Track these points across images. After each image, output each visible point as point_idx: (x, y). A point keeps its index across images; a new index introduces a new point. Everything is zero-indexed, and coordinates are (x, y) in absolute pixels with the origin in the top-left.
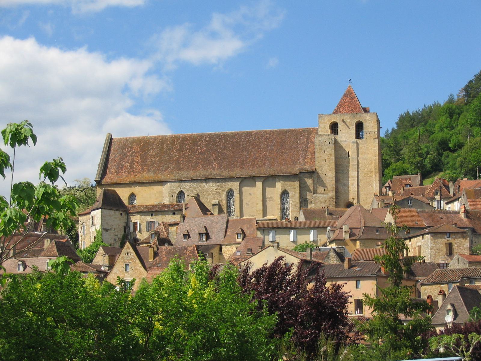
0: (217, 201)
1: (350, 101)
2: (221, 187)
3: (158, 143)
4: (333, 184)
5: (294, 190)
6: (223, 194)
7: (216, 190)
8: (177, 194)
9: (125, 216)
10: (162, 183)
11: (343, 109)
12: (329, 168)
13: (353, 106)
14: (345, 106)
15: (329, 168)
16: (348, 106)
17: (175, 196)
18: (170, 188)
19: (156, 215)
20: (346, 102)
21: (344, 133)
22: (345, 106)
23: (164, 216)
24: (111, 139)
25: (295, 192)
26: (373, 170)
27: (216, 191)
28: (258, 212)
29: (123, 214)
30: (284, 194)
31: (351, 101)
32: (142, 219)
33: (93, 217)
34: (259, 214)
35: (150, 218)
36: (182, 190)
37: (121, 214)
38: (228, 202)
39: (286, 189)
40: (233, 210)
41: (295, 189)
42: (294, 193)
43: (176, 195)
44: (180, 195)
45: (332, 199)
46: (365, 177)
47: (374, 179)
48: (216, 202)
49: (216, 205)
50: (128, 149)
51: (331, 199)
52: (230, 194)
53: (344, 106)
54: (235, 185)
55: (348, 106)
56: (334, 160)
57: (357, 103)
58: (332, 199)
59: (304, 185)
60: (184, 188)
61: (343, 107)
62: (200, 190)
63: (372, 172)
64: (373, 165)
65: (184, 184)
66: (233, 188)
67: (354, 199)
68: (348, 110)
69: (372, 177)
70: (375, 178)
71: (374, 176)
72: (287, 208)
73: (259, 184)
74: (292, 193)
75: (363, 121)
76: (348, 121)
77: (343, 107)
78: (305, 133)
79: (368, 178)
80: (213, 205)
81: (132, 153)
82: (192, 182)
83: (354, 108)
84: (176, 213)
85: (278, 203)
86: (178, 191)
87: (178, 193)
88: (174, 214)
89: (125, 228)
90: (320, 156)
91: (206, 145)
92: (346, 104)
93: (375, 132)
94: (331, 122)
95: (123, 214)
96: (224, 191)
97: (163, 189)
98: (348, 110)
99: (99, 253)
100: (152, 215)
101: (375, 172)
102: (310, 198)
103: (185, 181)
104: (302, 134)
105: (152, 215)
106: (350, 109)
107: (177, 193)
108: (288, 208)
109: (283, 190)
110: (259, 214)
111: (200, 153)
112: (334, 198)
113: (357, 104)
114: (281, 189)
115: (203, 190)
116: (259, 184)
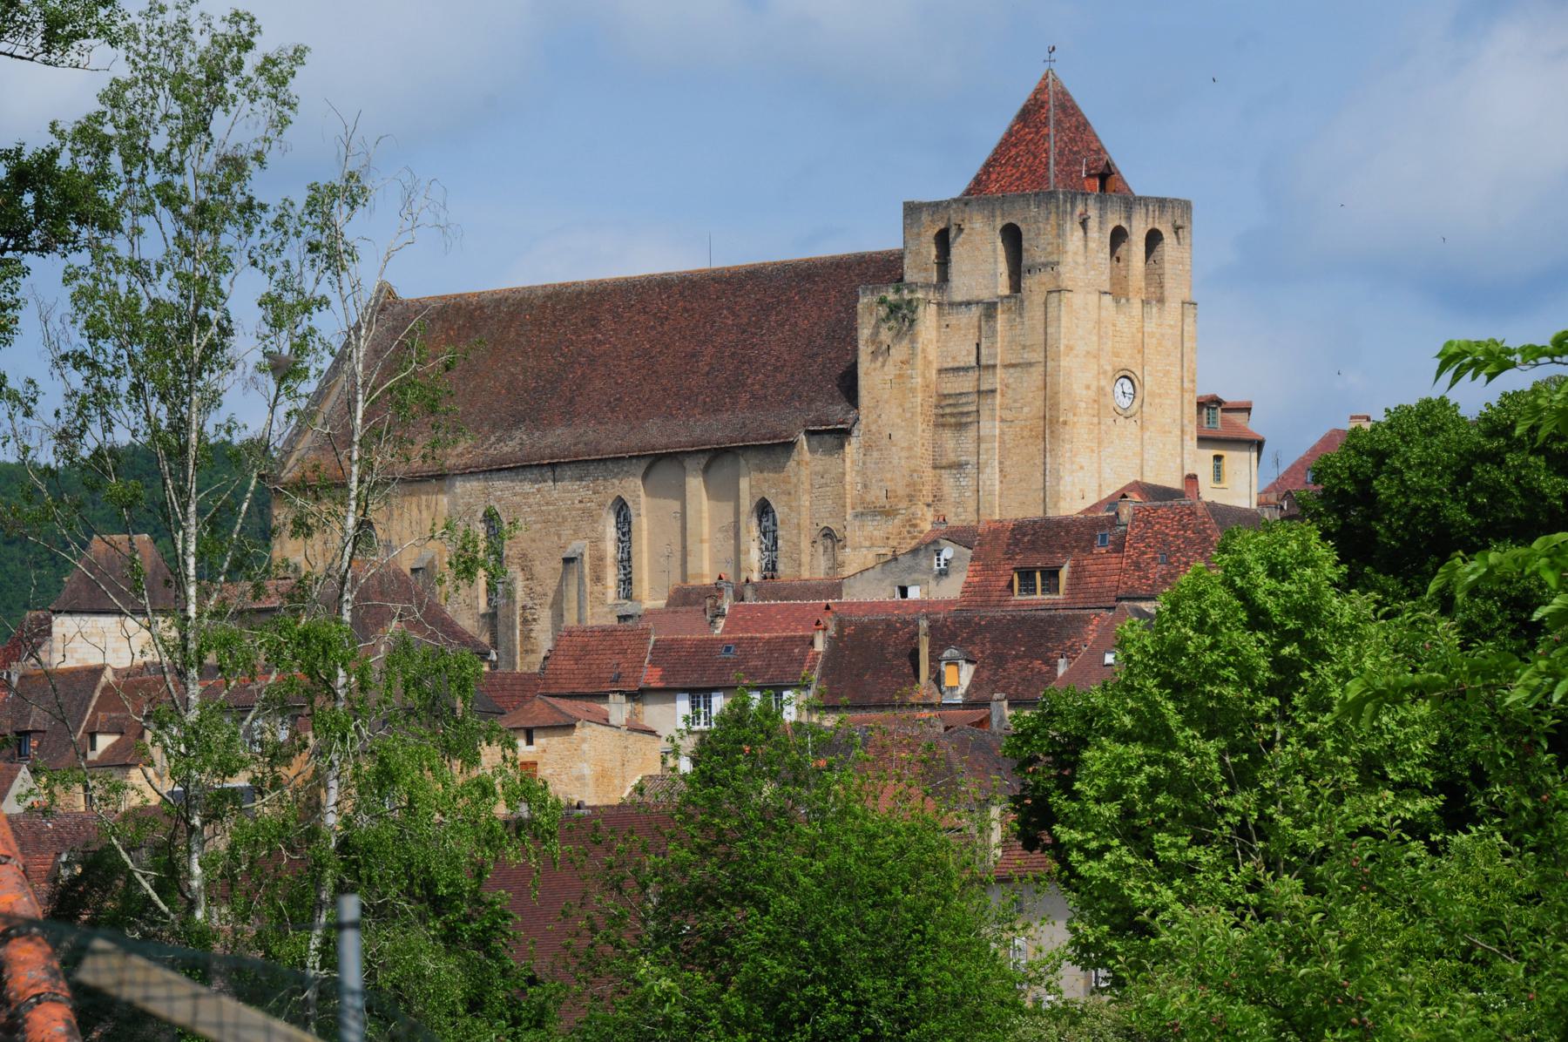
5: (785, 498)
7: (580, 502)
15: (900, 410)
27: (582, 505)
42: (786, 510)
51: (904, 526)
60: (499, 500)
83: (1030, 167)
109: (757, 499)
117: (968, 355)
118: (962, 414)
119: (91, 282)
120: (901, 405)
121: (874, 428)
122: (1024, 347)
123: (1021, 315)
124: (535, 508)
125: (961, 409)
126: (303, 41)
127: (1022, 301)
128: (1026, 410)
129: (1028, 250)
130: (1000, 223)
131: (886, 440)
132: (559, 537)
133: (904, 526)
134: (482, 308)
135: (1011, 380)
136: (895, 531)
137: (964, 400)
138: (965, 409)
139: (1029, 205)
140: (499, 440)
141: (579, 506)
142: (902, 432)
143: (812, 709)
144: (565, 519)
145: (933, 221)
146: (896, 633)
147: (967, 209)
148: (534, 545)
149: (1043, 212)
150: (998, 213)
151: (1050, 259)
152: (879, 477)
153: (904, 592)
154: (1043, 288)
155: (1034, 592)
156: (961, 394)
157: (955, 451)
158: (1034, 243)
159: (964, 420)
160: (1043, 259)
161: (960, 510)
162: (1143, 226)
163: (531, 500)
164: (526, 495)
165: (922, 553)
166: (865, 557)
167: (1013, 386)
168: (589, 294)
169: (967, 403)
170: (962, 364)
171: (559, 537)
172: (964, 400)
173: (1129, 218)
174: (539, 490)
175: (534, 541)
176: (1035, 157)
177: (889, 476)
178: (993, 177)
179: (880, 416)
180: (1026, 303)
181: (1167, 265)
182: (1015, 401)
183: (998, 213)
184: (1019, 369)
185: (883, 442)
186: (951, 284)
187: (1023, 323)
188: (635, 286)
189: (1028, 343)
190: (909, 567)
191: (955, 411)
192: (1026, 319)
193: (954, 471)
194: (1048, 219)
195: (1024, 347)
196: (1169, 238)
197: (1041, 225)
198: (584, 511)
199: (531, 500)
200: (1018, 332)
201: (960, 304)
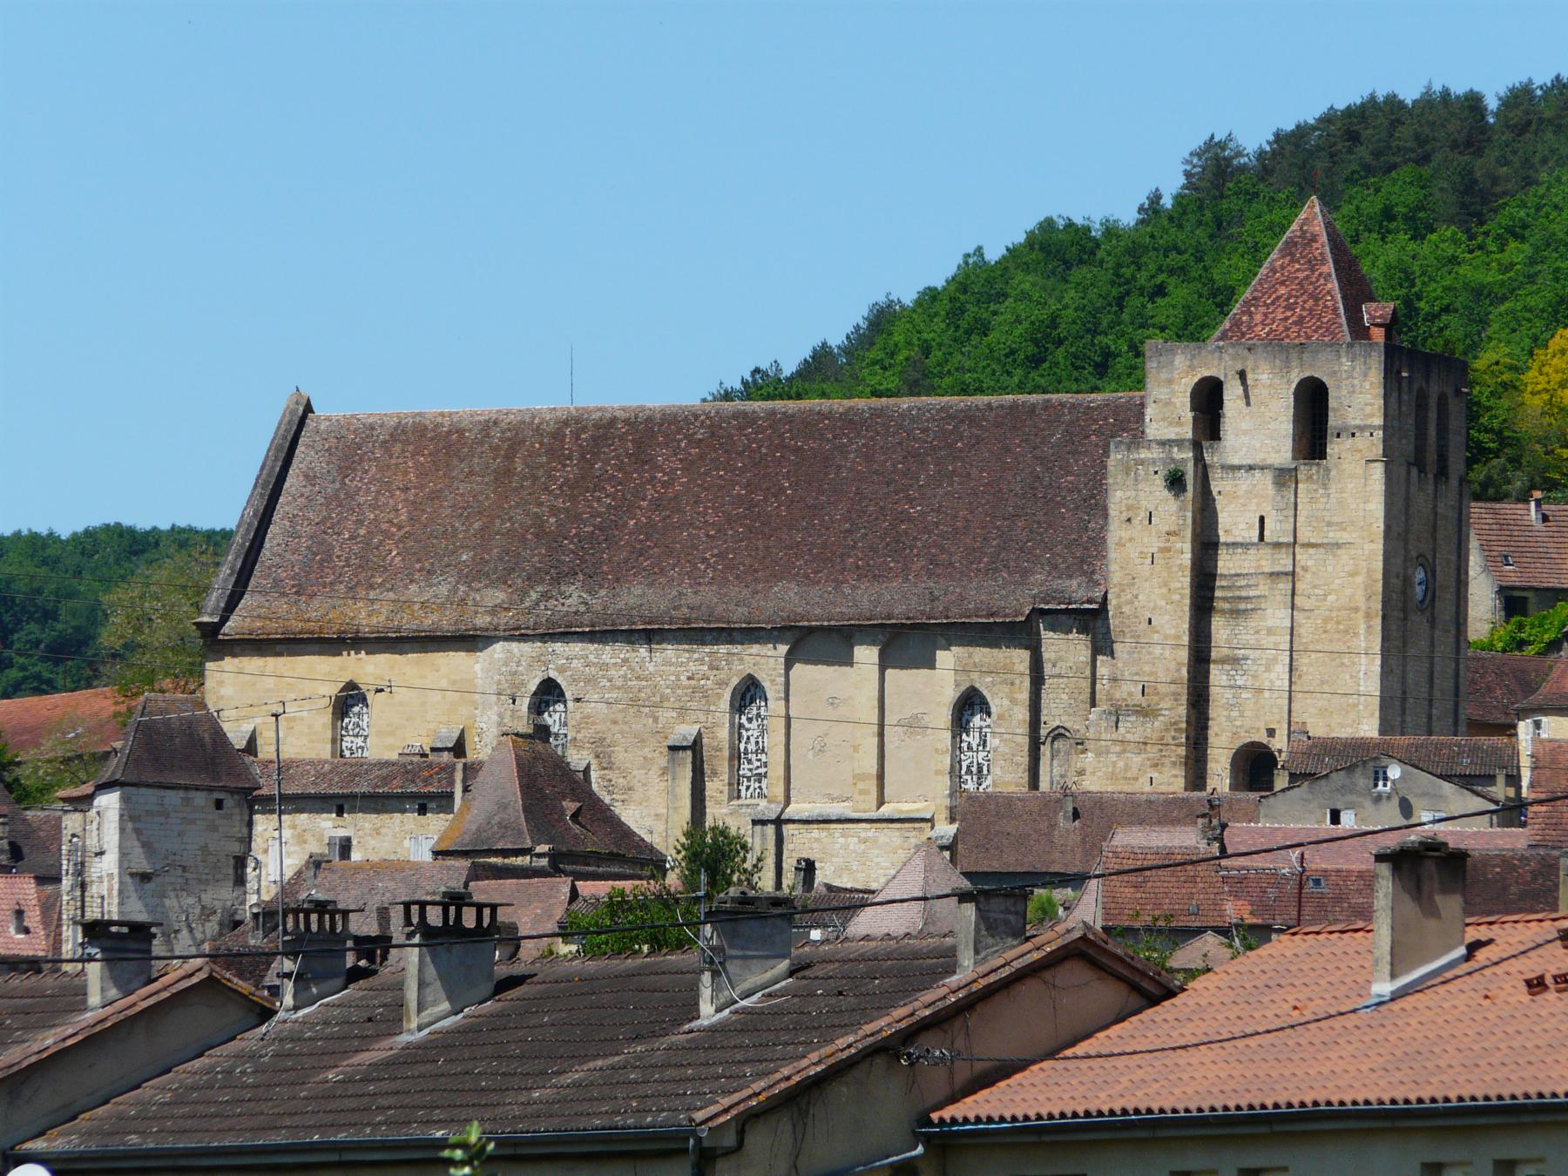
0: (694, 729)
2: (711, 668)
3: (495, 449)
5: (1006, 689)
6: (720, 696)
7: (689, 678)
8: (535, 694)
9: (237, 811)
10: (470, 641)
11: (1265, 315)
12: (1164, 590)
14: (1278, 298)
15: (1164, 590)
16: (1287, 299)
17: (524, 704)
18: (506, 664)
19: (352, 811)
20: (1283, 283)
21: (1245, 432)
23: (385, 817)
24: (308, 408)
25: (1014, 701)
26: (1361, 601)
27: (693, 682)
28: (861, 786)
29: (229, 802)
30: (969, 704)
31: (1307, 278)
32: (299, 830)
33: (98, 813)
34: (862, 792)
35: (329, 824)
36: (553, 674)
37: (219, 804)
38: (740, 735)
40: (762, 770)
41: (1012, 684)
42: (1006, 702)
43: (527, 701)
44: (546, 698)
45: (1173, 733)
46: (1325, 632)
48: (685, 731)
49: (684, 748)
50: (366, 472)
51: (1167, 730)
52: (748, 693)
53: (1273, 303)
54: (765, 661)
55: (1287, 299)
56: (1187, 558)
58: (1173, 733)
59: (1054, 666)
60: (561, 670)
61: (1268, 306)
62: (625, 677)
63: (1356, 609)
64: (1360, 579)
65: (558, 647)
66: (760, 676)
67: (1271, 733)
68: (1287, 319)
69: (1356, 634)
71: (1362, 628)
73: (866, 655)
74: (997, 701)
76: (1266, 376)
77: (1268, 306)
79: (1336, 636)
80: (673, 749)
81: (378, 492)
82: (592, 641)
83: (1311, 310)
84: (432, 805)
85: (939, 746)
86: (537, 681)
87: (538, 688)
88: (422, 810)
90: (1131, 539)
91: (688, 466)
92: (1283, 291)
93: (1375, 428)
94: (1196, 380)
95: (229, 802)
96: (722, 684)
97: (477, 667)
98: (1287, 319)
100: (340, 813)
101: (1368, 616)
103: (566, 636)
104: (1096, 421)
105: (340, 813)
106: (1295, 318)
107: (534, 689)
108: (985, 772)
109: (963, 688)
110: (862, 792)
111: (657, 505)
113: (1329, 293)
114: (957, 685)
115: (638, 678)
116: (866, 655)
118: (1240, 598)
122: (1329, 524)
123: (1325, 487)
124: (619, 683)
125: (1238, 593)
126: (1555, 74)
127: (1328, 470)
128: (1330, 598)
129: (1335, 410)
130: (1296, 377)
132: (656, 720)
133: (1167, 730)
134: (461, 432)
135: (1310, 563)
137: (1243, 582)
140: (546, 596)
141: (687, 683)
143: (1393, 976)
144: (664, 698)
145: (1192, 368)
148: (616, 728)
149: (1359, 367)
151: (1369, 422)
153: (1335, 818)
154: (1358, 456)
156: (1237, 575)
159: (1242, 606)
160: (1358, 422)
161: (1235, 714)
163: (612, 672)
164: (605, 667)
167: (1314, 569)
168: (627, 422)
169: (1248, 586)
170: (1239, 539)
171: (656, 720)
172: (1243, 582)
173: (1427, 382)
174: (625, 661)
175: (615, 722)
176: (1317, 300)
177: (1147, 668)
178: (1258, 318)
180: (1333, 473)
182: (1315, 587)
184: (1322, 550)
185: (1141, 627)
186: (1223, 443)
188: (696, 417)
189: (1335, 519)
193: (1228, 667)
194: (1366, 375)
196: (1232, 395)
197: (1356, 382)
198: (695, 690)
199: (612, 672)
201: (1239, 468)
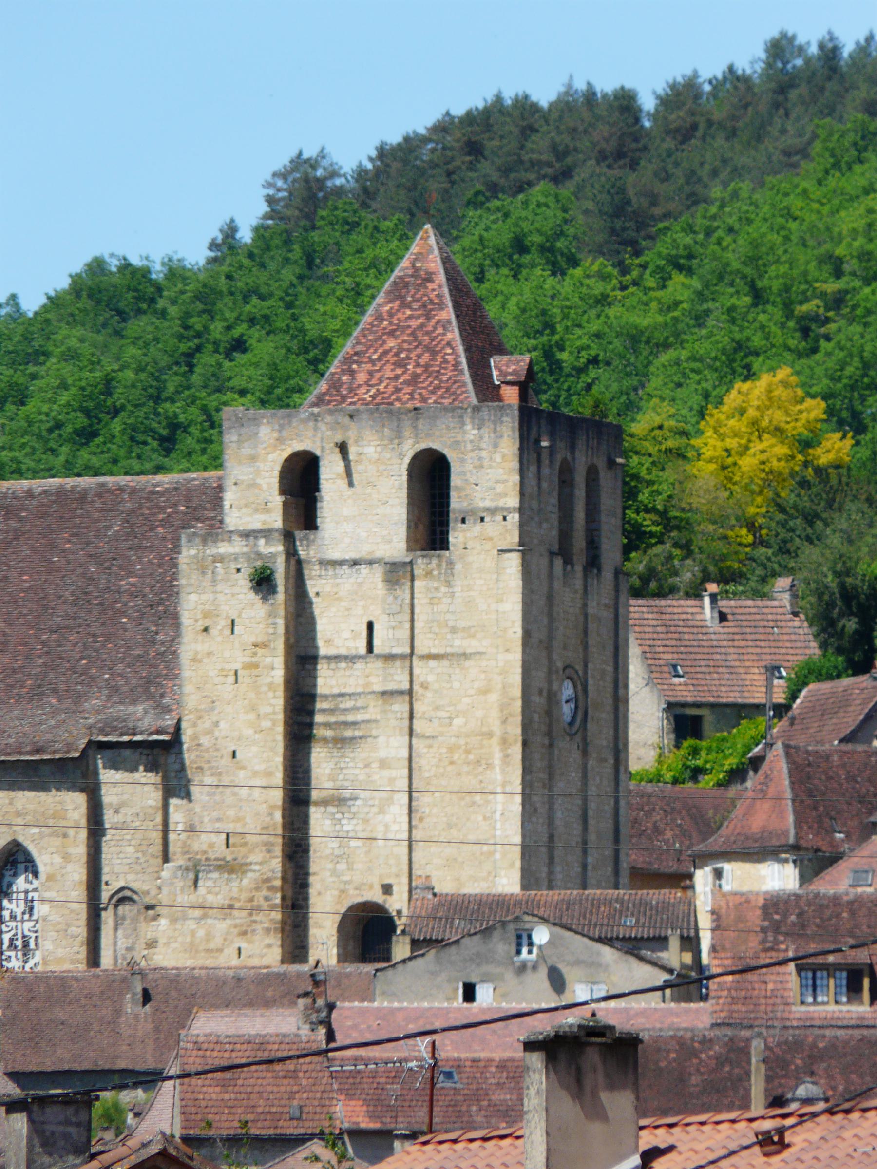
1: (414, 323)
4: (273, 807)
5: (57, 841)
11: (371, 373)
13: (426, 357)
14: (386, 353)
15: (252, 716)
16: (397, 354)
20: (392, 333)
22: (386, 353)
25: (67, 857)
39: (20, 839)
41: (65, 836)
42: (57, 859)
45: (265, 893)
46: (452, 763)
47: (499, 777)
51: (257, 889)
53: (380, 359)
55: (397, 354)
56: (278, 674)
57: (449, 336)
61: (372, 362)
63: (490, 735)
64: (494, 697)
67: (387, 889)
68: (397, 377)
69: (490, 766)
70: (503, 772)
72: (26, 945)
75: (446, 452)
77: (372, 362)
78: (176, 505)
79: (466, 768)
83: (427, 367)
89: (464, 654)
90: (209, 654)
92: (391, 343)
93: (508, 510)
98: (397, 377)
99: (515, 742)
102: (145, 888)
106: (406, 377)
108: (32, 945)
112: (278, 883)
113: (449, 344)
117: (354, 638)
118: (346, 724)
119: (837, 535)
120: (253, 708)
121: (205, 741)
122: (454, 630)
123: (449, 584)
125: (342, 718)
127: (451, 563)
130: (410, 449)
131: (227, 760)
133: (257, 889)
136: (244, 896)
138: (350, 718)
139: (463, 424)
142: (254, 749)
146: (697, 1057)
147: (353, 425)
150: (407, 432)
151: (501, 503)
152: (215, 814)
153: (469, 994)
155: (861, 1003)
156: (342, 695)
157: (331, 777)
158: (473, 480)
159: (348, 733)
160: (488, 504)
161: (342, 866)
162: (584, 459)
165: (497, 935)
166: (193, 933)
167: (436, 686)
170: (343, 651)
173: (573, 453)
176: (434, 353)
177: (231, 813)
178: (361, 377)
179: (217, 724)
180: (458, 567)
181: (603, 518)
182: (437, 708)
183: (407, 432)
184: (445, 663)
186: (320, 534)
187: (452, 595)
189: (461, 624)
190: (478, 955)
191: (332, 719)
192: (457, 589)
194: (496, 446)
195: (454, 630)
197: (484, 454)
200: (443, 607)
